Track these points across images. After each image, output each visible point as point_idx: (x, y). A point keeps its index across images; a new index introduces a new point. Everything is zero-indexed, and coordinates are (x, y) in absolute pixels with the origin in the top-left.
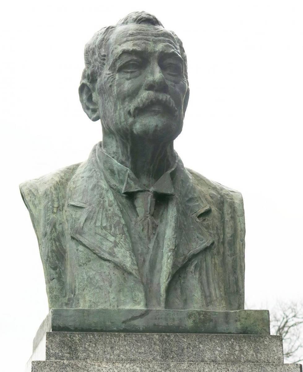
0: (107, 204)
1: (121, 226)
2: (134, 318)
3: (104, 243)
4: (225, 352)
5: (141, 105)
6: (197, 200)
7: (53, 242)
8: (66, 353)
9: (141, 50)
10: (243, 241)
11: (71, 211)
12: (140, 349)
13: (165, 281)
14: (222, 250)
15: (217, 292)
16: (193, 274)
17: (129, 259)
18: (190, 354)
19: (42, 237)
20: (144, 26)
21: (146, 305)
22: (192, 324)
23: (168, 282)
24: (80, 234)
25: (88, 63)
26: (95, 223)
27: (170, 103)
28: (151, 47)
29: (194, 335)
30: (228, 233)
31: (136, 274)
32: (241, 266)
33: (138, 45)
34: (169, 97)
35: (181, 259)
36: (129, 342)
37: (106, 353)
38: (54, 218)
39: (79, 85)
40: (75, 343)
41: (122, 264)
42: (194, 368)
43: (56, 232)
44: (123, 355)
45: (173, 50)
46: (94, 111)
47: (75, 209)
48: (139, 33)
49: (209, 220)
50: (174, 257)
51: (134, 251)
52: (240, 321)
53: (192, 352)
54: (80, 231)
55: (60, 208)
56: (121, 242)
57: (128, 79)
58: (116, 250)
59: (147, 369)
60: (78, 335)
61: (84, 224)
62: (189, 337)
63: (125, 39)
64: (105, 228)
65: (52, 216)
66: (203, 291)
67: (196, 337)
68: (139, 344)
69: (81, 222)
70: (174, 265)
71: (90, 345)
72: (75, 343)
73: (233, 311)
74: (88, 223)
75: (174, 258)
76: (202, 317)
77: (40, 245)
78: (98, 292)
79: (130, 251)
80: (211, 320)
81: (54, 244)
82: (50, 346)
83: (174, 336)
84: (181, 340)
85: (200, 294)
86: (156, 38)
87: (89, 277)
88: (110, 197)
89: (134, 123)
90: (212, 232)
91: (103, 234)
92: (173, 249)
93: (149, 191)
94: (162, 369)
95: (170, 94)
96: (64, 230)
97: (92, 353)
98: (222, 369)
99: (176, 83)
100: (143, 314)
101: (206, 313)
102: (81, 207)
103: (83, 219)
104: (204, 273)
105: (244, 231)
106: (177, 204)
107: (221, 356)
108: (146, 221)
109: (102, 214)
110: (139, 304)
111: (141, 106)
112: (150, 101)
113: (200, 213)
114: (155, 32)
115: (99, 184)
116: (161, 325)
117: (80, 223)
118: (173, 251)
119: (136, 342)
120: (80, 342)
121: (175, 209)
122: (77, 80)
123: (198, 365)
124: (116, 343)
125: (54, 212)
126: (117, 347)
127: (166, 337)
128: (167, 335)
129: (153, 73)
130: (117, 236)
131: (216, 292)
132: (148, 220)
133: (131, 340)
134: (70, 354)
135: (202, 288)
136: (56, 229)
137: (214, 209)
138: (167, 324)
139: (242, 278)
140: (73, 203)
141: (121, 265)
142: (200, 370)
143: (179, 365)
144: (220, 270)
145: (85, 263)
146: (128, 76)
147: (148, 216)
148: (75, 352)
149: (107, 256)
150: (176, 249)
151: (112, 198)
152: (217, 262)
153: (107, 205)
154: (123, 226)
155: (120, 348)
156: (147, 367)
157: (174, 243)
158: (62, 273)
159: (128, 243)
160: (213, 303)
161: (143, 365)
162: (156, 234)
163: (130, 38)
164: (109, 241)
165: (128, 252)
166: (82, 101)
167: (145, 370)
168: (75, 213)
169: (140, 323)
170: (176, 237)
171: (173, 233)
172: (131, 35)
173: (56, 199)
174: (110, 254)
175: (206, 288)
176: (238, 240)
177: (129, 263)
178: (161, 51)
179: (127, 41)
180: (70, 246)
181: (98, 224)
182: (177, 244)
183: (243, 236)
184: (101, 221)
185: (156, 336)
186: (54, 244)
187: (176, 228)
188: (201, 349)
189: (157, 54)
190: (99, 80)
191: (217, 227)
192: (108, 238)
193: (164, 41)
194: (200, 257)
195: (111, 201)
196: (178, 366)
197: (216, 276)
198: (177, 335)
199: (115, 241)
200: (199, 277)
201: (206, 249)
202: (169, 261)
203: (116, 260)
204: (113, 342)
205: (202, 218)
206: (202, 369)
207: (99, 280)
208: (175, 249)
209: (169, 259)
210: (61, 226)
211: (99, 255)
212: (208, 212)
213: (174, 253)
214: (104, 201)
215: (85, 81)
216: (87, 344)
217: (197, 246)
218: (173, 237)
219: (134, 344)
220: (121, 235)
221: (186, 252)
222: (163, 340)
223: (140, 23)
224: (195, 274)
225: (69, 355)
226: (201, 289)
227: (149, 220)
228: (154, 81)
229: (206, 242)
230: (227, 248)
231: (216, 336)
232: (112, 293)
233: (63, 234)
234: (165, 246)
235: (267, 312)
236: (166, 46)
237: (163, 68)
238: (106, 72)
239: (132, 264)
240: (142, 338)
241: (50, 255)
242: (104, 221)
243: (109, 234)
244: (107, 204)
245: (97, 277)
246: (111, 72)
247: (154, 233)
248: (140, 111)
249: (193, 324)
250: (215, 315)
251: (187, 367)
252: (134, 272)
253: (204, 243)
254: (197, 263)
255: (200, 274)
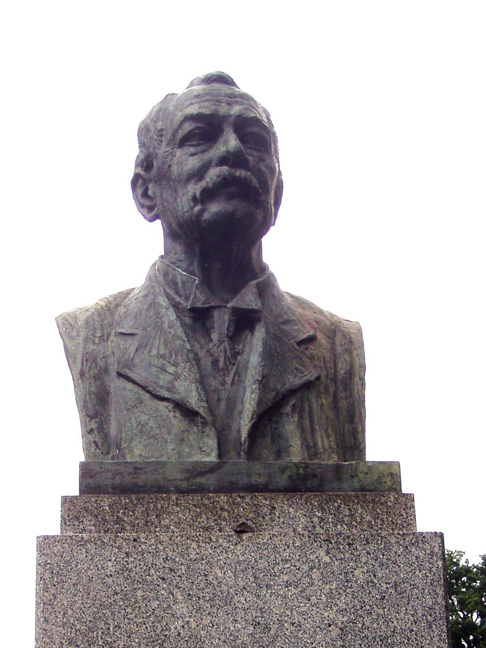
0: (166, 325)
1: (186, 351)
2: (201, 474)
3: (162, 376)
4: (328, 519)
5: (211, 186)
6: (296, 324)
7: (93, 381)
8: (90, 526)
9: (209, 113)
10: (362, 379)
11: (121, 341)
12: (199, 517)
13: (247, 422)
14: (332, 389)
15: (326, 442)
16: (290, 417)
17: (194, 394)
18: (275, 522)
19: (81, 376)
20: (216, 86)
21: (220, 456)
22: (287, 481)
23: (251, 424)
24: (129, 369)
25: (142, 145)
26: (150, 352)
27: (251, 182)
28: (223, 109)
29: (281, 495)
30: (341, 369)
31: (204, 412)
32: (360, 413)
33: (205, 107)
34: (249, 173)
35: (271, 396)
36: (183, 508)
37: (149, 524)
38: (94, 350)
39: (131, 176)
40: (103, 510)
41: (185, 401)
42: (278, 540)
43: (97, 367)
44: (174, 526)
45: (254, 115)
46: (150, 209)
47: (124, 337)
48: (207, 94)
49: (312, 349)
50: (261, 391)
51: (202, 382)
52: (357, 476)
53: (278, 520)
54: (129, 364)
55: (105, 338)
56: (184, 373)
57: (192, 155)
58: (176, 384)
59: (208, 544)
60: (108, 499)
61: (134, 355)
62: (273, 498)
63: (189, 102)
64: (163, 357)
65: (92, 347)
66: (304, 439)
67: (283, 498)
68: (198, 510)
69: (131, 352)
70: (259, 403)
71: (125, 513)
72: (103, 510)
73: (347, 463)
74: (139, 353)
75: (260, 392)
76: (301, 471)
77: (75, 387)
78: (152, 442)
79: (196, 384)
80: (315, 476)
81: (93, 384)
82: (66, 515)
83: (250, 497)
84: (261, 502)
85: (299, 442)
86: (231, 99)
87: (140, 423)
88: (171, 315)
89: (202, 212)
90: (317, 363)
91: (159, 365)
92: (259, 380)
93: (225, 307)
94: (230, 543)
95: (251, 171)
96: (108, 365)
97: (128, 524)
98: (322, 541)
99: (262, 160)
100: (212, 469)
101: (307, 466)
102: (131, 334)
103: (133, 349)
104: (306, 415)
105: (363, 367)
106: (266, 323)
107: (322, 525)
108: (222, 347)
109: (159, 339)
110: (209, 455)
111: (210, 187)
112: (221, 178)
113: (300, 339)
114: (229, 92)
115: (157, 301)
116: (241, 484)
117: (129, 354)
118: (259, 383)
119: (194, 508)
120: (110, 509)
121: (263, 330)
122: (129, 170)
123: (284, 536)
124: (164, 509)
125: (96, 343)
126: (165, 515)
127: (239, 499)
128: (240, 497)
129: (226, 142)
130: (179, 365)
131: (323, 442)
132: (225, 346)
133: (185, 505)
134: (96, 527)
135: (304, 436)
136: (96, 364)
137: (320, 336)
138: (250, 481)
139: (362, 428)
140: (122, 331)
141: (183, 402)
142: (288, 544)
143: (256, 537)
144: (331, 414)
145: (135, 406)
146: (192, 150)
147: (224, 340)
148: (103, 523)
149: (166, 394)
150: (264, 381)
151: (173, 317)
152: (324, 402)
153: (167, 327)
154: (188, 351)
155: (170, 516)
156: (207, 540)
157: (261, 373)
158: (104, 423)
159: (194, 373)
160: (319, 456)
161: (202, 538)
162: (237, 364)
163: (194, 101)
164: (169, 372)
165: (194, 385)
166: (136, 198)
167: (204, 545)
168: (123, 342)
169: (210, 480)
170: (264, 365)
171: (260, 360)
172: (198, 96)
173: (99, 327)
174: (169, 390)
175: (309, 437)
176: (357, 379)
177: (194, 400)
178: (237, 114)
179: (192, 104)
180: (116, 385)
181: (154, 352)
182: (265, 375)
183: (363, 373)
184: (158, 347)
185: (223, 498)
186: (93, 384)
187: (264, 354)
188: (291, 516)
189: (232, 119)
190: (155, 163)
191: (324, 359)
192: (167, 369)
193: (242, 104)
194: (299, 395)
195: (172, 321)
196: (255, 539)
197: (323, 420)
198: (255, 496)
199: (176, 372)
200: (298, 421)
201: (308, 385)
202: (253, 395)
203: (177, 397)
204: (159, 507)
205: (303, 346)
206: (291, 542)
207: (154, 426)
208: (262, 380)
209: (253, 393)
210: (104, 360)
211: (154, 392)
212: (312, 339)
213: (261, 385)
214: (162, 323)
215: (139, 171)
216: (121, 511)
217: (294, 381)
218: (260, 365)
219: (190, 510)
220: (185, 363)
221: (279, 386)
222: (234, 503)
223: (209, 84)
224: (292, 416)
225: (94, 527)
226: (301, 436)
227: (227, 345)
228: (228, 152)
229: (309, 374)
230: (341, 388)
231: (315, 495)
232: (171, 442)
233: (106, 370)
234: (249, 377)
235: (397, 464)
236: (245, 109)
237: (242, 138)
238: (163, 149)
239: (198, 400)
240: (203, 501)
241: (88, 398)
242: (162, 348)
243: (168, 363)
244: (166, 325)
245: (151, 423)
246: (169, 149)
247: (233, 362)
248: (208, 195)
249: (288, 482)
250: (321, 468)
251: (268, 540)
252: (201, 411)
253: (306, 375)
254: (295, 403)
255: (301, 417)
